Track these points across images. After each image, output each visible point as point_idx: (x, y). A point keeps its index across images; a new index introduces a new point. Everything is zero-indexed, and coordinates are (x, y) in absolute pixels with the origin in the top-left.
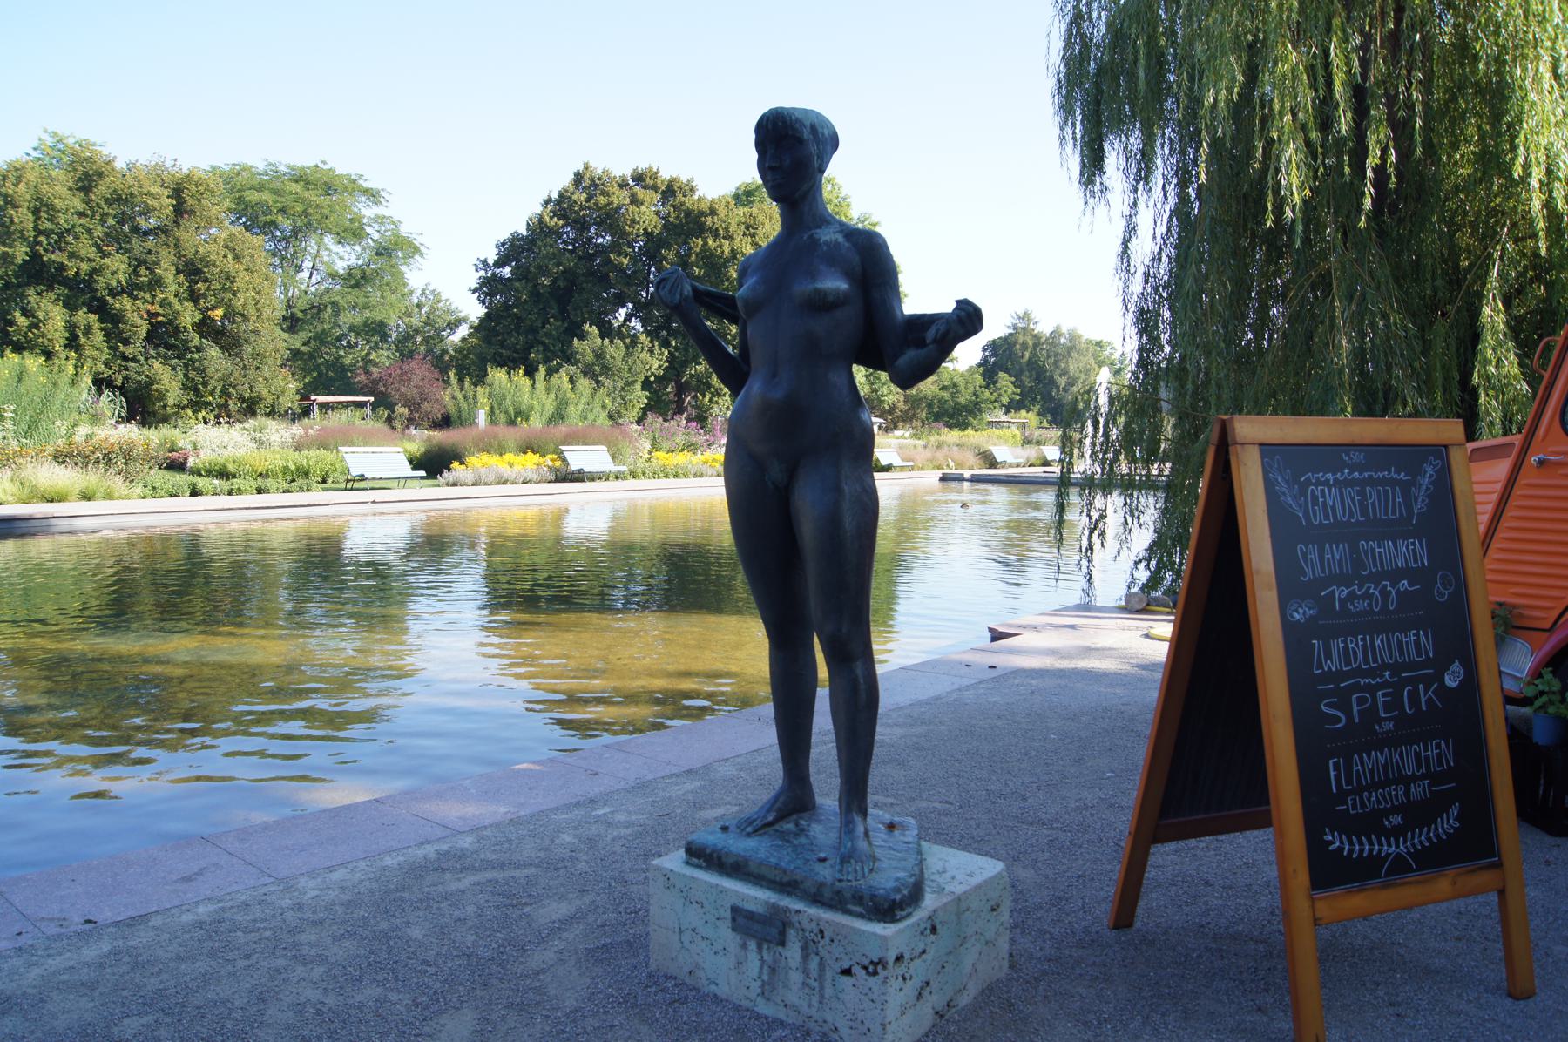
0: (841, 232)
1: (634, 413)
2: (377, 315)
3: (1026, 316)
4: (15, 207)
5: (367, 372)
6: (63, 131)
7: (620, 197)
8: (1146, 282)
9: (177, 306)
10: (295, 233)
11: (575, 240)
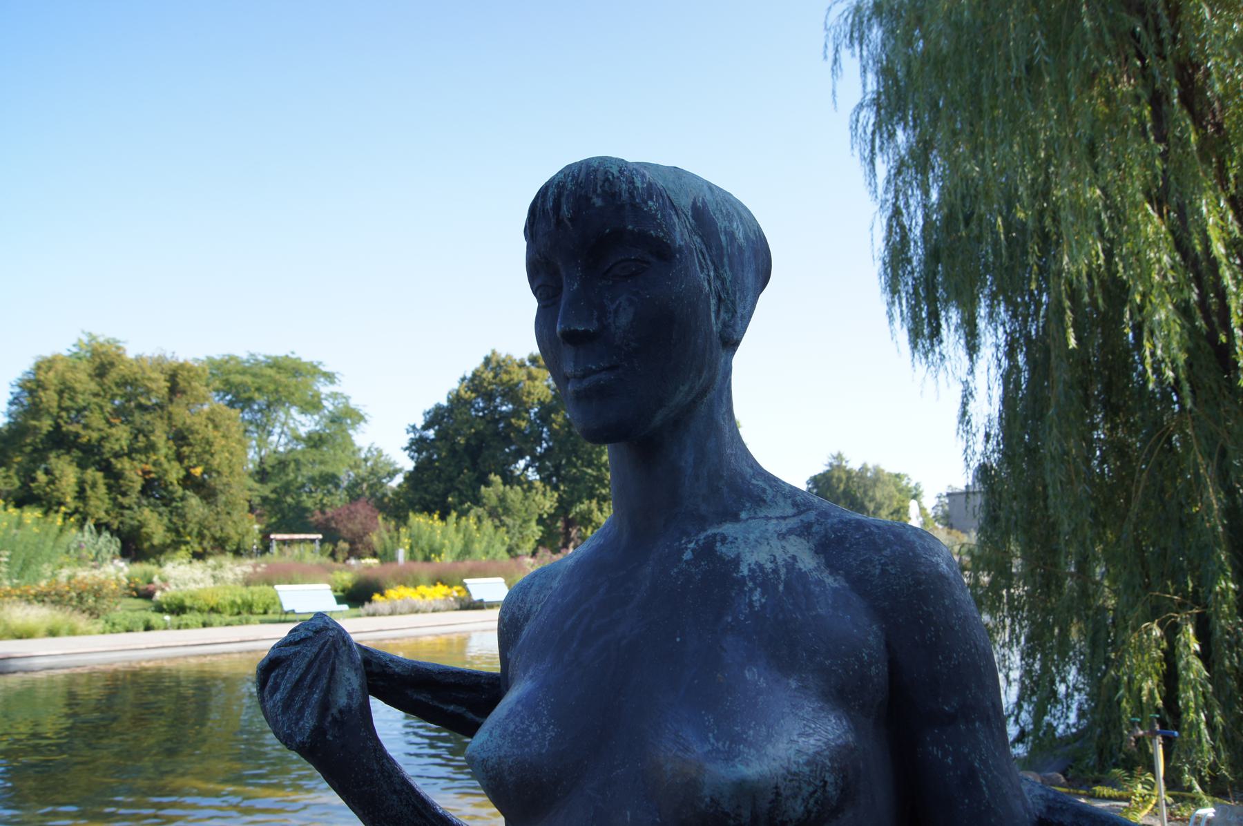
0: (804, 531)
1: (529, 546)
2: (329, 469)
3: (839, 457)
5: (323, 512)
6: (95, 332)
7: (519, 375)
8: (987, 441)
9: (166, 466)
10: (268, 406)
11: (483, 409)
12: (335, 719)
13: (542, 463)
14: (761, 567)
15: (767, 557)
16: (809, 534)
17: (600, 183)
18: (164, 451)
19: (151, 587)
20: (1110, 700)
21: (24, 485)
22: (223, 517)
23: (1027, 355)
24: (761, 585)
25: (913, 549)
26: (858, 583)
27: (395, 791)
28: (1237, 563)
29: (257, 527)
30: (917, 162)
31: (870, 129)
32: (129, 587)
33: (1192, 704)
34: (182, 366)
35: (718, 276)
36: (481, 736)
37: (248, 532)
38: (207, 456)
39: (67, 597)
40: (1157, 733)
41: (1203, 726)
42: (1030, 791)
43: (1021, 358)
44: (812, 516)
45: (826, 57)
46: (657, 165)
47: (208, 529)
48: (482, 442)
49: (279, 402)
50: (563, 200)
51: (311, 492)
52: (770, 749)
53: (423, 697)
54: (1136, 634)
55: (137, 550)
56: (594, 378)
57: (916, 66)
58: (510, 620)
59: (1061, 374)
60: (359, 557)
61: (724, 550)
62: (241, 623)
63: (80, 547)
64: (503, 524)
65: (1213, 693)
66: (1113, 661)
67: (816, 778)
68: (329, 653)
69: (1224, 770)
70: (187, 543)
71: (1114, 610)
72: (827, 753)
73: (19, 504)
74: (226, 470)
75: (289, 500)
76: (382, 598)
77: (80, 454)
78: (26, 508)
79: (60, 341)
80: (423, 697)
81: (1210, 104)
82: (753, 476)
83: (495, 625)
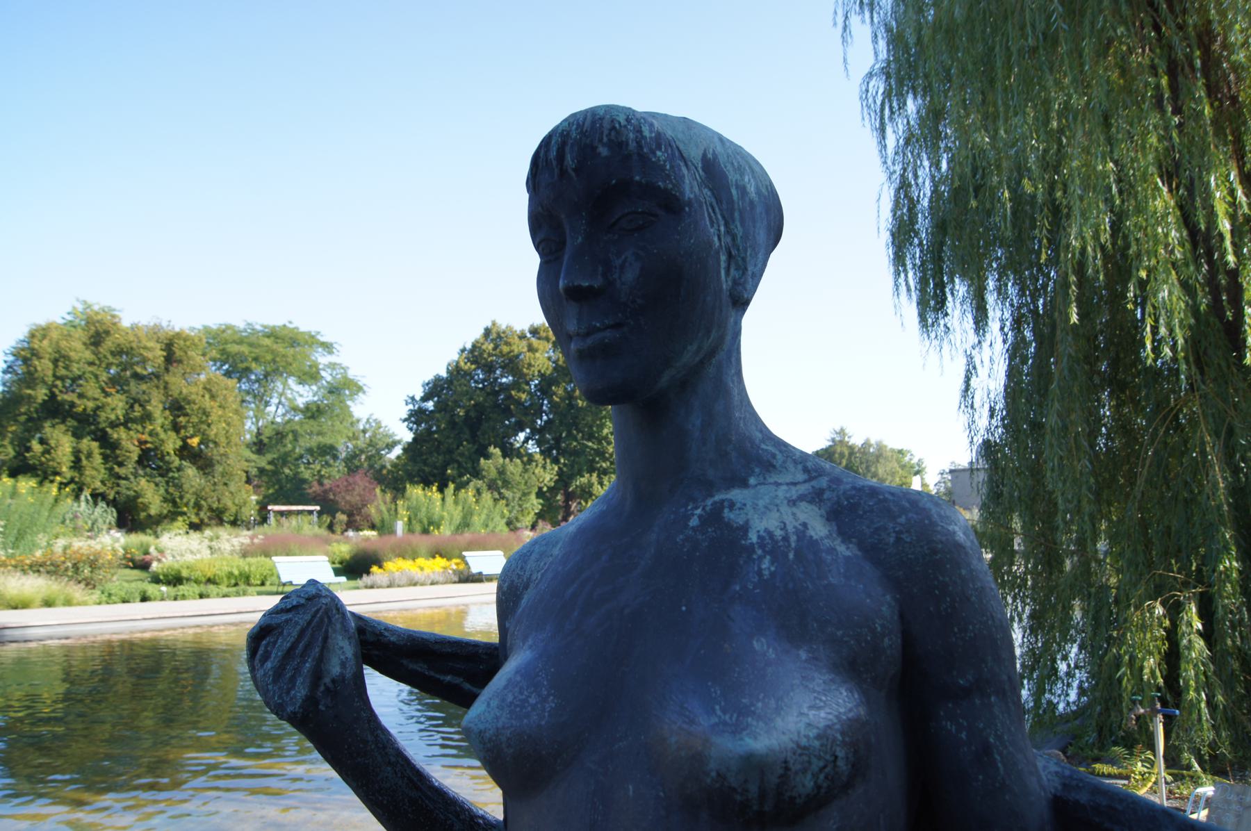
0: (816, 497)
1: (528, 519)
2: (327, 440)
3: (842, 432)
4: (39, 358)
5: (321, 484)
6: (90, 300)
7: (519, 347)
8: (992, 416)
9: (163, 436)
10: (266, 377)
11: (483, 381)
12: (327, 689)
13: (542, 436)
14: (770, 534)
15: (777, 524)
16: (821, 500)
17: (606, 132)
18: (160, 421)
19: (148, 558)
20: (1110, 677)
21: (19, 454)
22: (220, 487)
23: (1033, 330)
24: (770, 553)
25: (929, 517)
26: (872, 551)
27: (389, 763)
28: (1243, 543)
29: (254, 498)
30: (925, 136)
31: (879, 99)
32: (125, 558)
33: (1192, 683)
34: (178, 335)
35: (729, 232)
36: (478, 708)
37: (245, 503)
38: (204, 427)
39: (62, 568)
40: (1159, 711)
41: (1203, 705)
42: (1045, 768)
43: (1028, 334)
44: (823, 482)
45: (835, 24)
46: (666, 116)
47: (205, 500)
48: (482, 414)
49: (276, 371)
50: (568, 149)
51: (309, 463)
52: (779, 722)
53: (419, 667)
54: (1138, 613)
55: (133, 520)
56: (599, 335)
57: (927, 33)
58: (510, 588)
59: (1067, 347)
60: (358, 529)
61: (732, 516)
62: (238, 594)
63: (76, 517)
64: (502, 497)
65: (1215, 672)
66: (1115, 639)
67: (826, 753)
68: (322, 620)
69: (1224, 750)
70: (184, 514)
71: (1117, 588)
72: (838, 727)
73: (13, 474)
74: (223, 440)
75: (287, 471)
76: (380, 571)
77: (75, 424)
78: (20, 477)
79: (55, 310)
80: (419, 667)
81: (1226, 76)
82: (763, 441)
83: (494, 597)
